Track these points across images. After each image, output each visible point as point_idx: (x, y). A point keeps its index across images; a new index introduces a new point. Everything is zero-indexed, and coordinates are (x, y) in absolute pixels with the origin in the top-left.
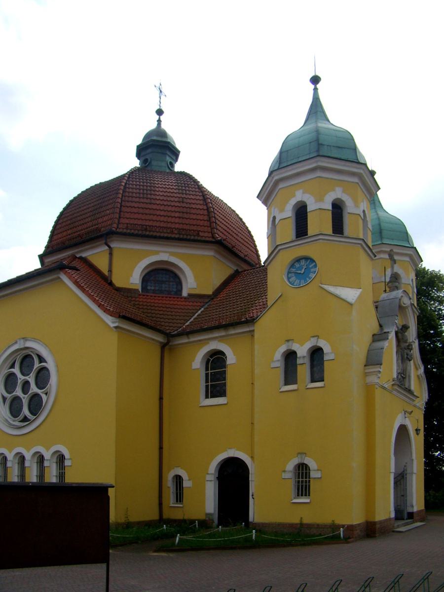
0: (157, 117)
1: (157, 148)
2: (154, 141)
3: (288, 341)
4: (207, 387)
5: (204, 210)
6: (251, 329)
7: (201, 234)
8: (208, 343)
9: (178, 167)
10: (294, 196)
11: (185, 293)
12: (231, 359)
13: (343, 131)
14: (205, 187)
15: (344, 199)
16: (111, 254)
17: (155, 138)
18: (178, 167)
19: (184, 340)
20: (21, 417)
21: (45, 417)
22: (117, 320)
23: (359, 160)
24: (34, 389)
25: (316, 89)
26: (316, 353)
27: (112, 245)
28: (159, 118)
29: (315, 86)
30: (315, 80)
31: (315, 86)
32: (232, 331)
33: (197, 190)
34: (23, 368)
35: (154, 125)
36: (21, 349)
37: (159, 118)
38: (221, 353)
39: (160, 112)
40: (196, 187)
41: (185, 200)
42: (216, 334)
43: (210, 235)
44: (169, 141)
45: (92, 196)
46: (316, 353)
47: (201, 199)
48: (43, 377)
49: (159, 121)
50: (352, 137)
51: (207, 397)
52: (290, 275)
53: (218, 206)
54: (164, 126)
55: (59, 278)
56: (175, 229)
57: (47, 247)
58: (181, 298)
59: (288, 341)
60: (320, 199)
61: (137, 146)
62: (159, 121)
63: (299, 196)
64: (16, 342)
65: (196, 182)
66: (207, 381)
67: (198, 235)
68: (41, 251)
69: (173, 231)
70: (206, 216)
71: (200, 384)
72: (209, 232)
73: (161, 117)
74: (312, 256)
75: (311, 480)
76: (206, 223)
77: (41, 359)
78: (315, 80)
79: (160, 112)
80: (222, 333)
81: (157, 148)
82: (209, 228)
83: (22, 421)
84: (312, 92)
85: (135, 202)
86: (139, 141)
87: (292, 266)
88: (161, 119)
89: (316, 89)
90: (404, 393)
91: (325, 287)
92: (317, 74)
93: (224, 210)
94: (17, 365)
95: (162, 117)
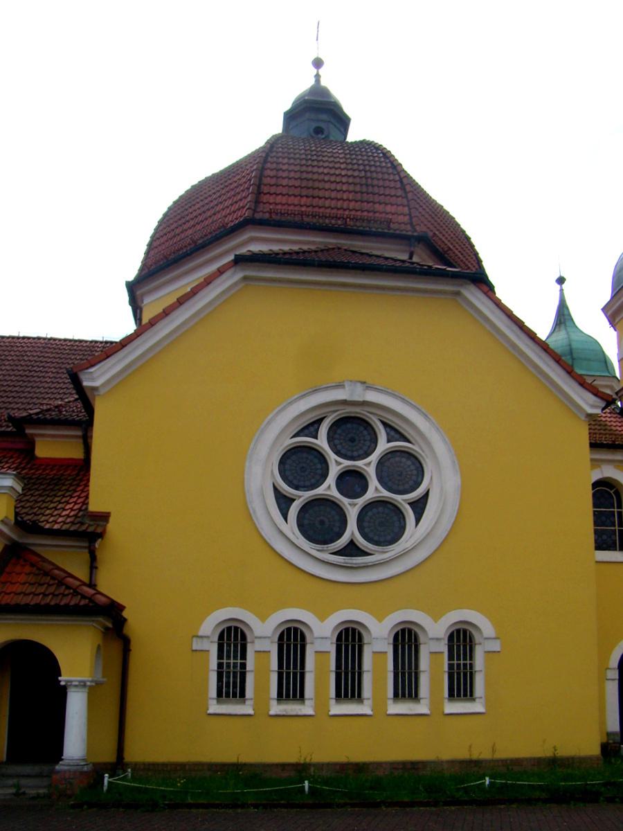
0: (315, 71)
5: (396, 181)
9: (353, 136)
14: (406, 169)
17: (306, 98)
18: (353, 136)
25: (561, 290)
26: (461, 641)
28: (318, 71)
29: (561, 287)
30: (561, 281)
31: (561, 287)
33: (390, 171)
34: (294, 457)
35: (312, 82)
37: (318, 71)
39: (318, 63)
40: (389, 165)
43: (406, 219)
44: (333, 100)
45: (214, 189)
46: (461, 641)
49: (318, 77)
53: (450, 232)
55: (458, 294)
56: (350, 219)
57: (141, 270)
61: (285, 113)
62: (318, 77)
65: (395, 166)
68: (132, 275)
69: (346, 223)
70: (399, 190)
72: (404, 206)
77: (395, 433)
78: (561, 281)
79: (318, 63)
81: (317, 115)
82: (406, 208)
84: (558, 293)
85: (283, 186)
86: (288, 106)
89: (561, 290)
90: (54, 543)
92: (562, 275)
93: (460, 240)
94: (323, 430)
95: (321, 72)
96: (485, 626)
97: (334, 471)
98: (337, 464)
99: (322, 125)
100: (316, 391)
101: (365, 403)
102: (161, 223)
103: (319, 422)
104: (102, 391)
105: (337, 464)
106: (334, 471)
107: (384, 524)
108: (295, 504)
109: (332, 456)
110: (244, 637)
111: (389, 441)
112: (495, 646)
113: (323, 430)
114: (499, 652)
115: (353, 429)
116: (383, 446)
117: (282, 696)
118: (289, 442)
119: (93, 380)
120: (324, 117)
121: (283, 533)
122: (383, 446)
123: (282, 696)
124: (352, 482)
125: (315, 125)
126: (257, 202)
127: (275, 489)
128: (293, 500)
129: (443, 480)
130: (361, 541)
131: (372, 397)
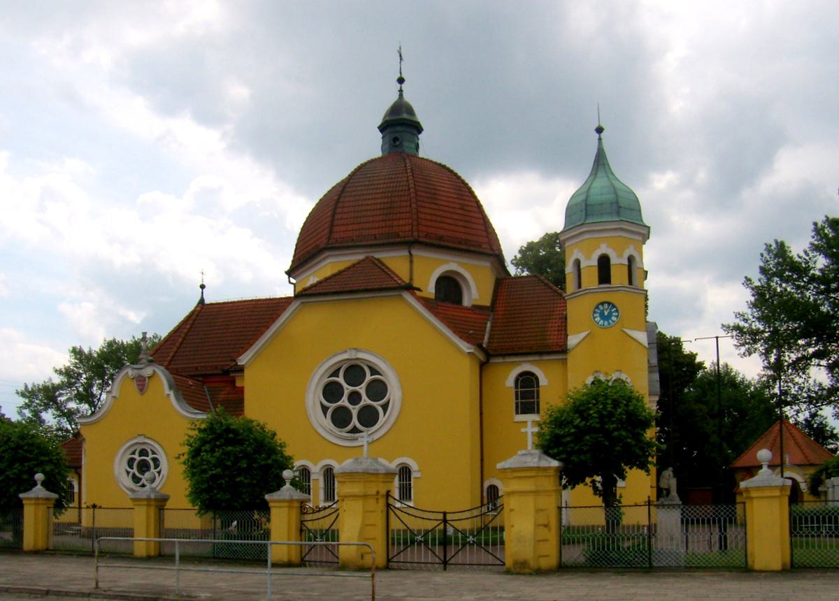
1: (697, 354)
2: (405, 119)
3: (596, 372)
4: (517, 404)
6: (564, 357)
7: (483, 246)
8: (521, 365)
10: (599, 247)
11: (466, 302)
12: (543, 381)
13: (626, 191)
15: (635, 255)
16: (411, 262)
19: (500, 360)
20: (350, 427)
21: (389, 427)
22: (472, 347)
23: (644, 220)
24: (365, 400)
25: (600, 139)
27: (414, 252)
28: (401, 87)
32: (546, 357)
35: (395, 97)
36: (348, 359)
37: (401, 87)
38: (532, 374)
41: (465, 207)
42: (531, 358)
47: (420, 203)
48: (378, 390)
49: (401, 91)
50: (637, 198)
51: (517, 413)
52: (595, 315)
54: (407, 98)
55: (401, 295)
58: (461, 309)
59: (596, 372)
60: (620, 256)
62: (401, 91)
63: (604, 249)
64: (346, 352)
66: (517, 399)
67: (480, 246)
71: (511, 401)
73: (403, 85)
74: (616, 304)
75: (617, 489)
76: (419, 193)
77: (374, 371)
79: (401, 81)
80: (537, 358)
81: (697, 354)
83: (351, 432)
87: (597, 307)
88: (403, 89)
89: (600, 139)
91: (625, 330)
94: (341, 373)
96: (414, 466)
97: (346, 393)
98: (348, 389)
99: (397, 135)
100: (335, 355)
101: (357, 359)
102: (308, 218)
103: (339, 369)
104: (247, 365)
105: (348, 389)
106: (346, 393)
107: (369, 417)
108: (329, 410)
109: (345, 385)
110: (309, 473)
111: (372, 375)
112: (418, 475)
113: (341, 373)
114: (625, 487)
115: (354, 372)
116: (369, 378)
117: (327, 500)
118: (326, 380)
119: (241, 362)
120: (399, 128)
121: (324, 423)
122: (369, 378)
123: (327, 500)
124: (355, 398)
125: (393, 136)
126: (331, 232)
127: (321, 403)
128: (329, 408)
129: (395, 393)
130: (358, 426)
131: (361, 355)
